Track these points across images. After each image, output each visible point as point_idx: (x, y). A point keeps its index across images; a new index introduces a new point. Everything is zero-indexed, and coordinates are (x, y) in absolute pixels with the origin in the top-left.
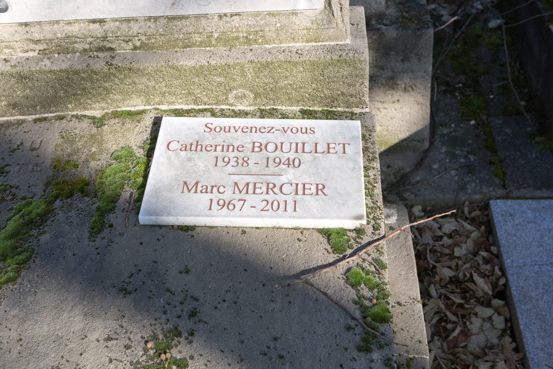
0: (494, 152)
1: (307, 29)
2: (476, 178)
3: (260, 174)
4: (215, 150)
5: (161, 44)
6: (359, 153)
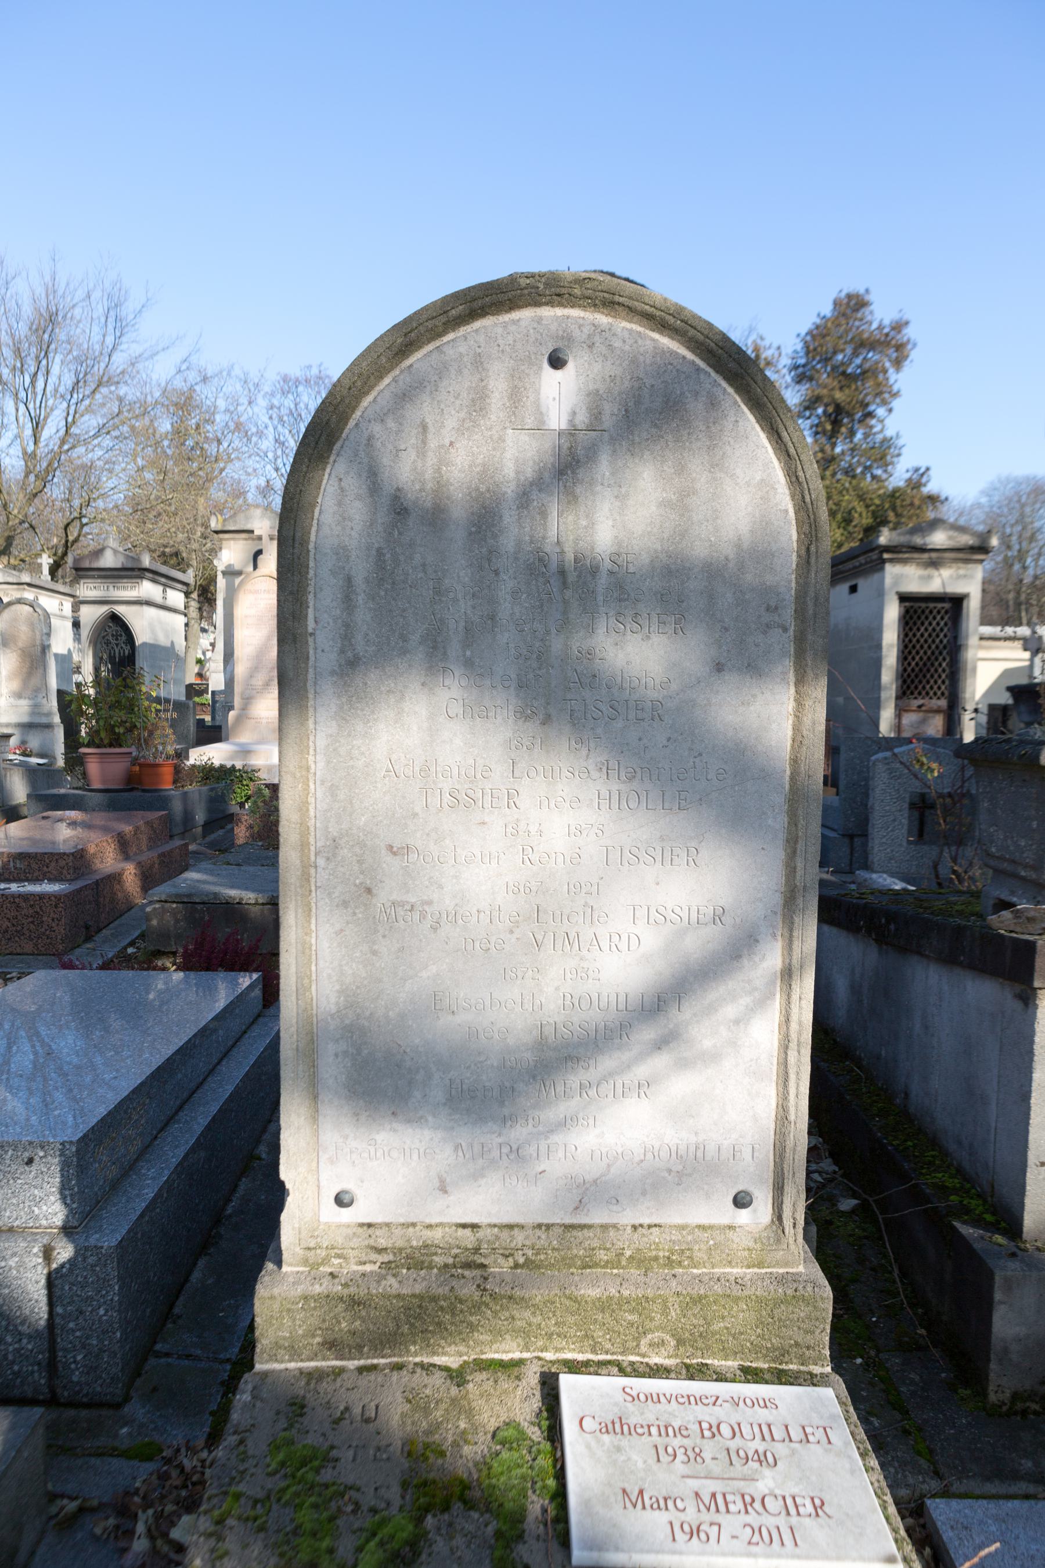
0: (905, 1413)
1: (749, 1249)
2: (893, 1458)
3: (726, 1476)
4: (650, 1434)
5: (552, 1261)
6: (850, 1443)
